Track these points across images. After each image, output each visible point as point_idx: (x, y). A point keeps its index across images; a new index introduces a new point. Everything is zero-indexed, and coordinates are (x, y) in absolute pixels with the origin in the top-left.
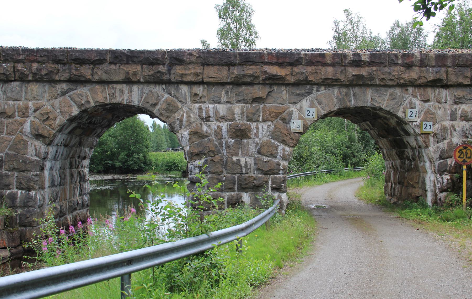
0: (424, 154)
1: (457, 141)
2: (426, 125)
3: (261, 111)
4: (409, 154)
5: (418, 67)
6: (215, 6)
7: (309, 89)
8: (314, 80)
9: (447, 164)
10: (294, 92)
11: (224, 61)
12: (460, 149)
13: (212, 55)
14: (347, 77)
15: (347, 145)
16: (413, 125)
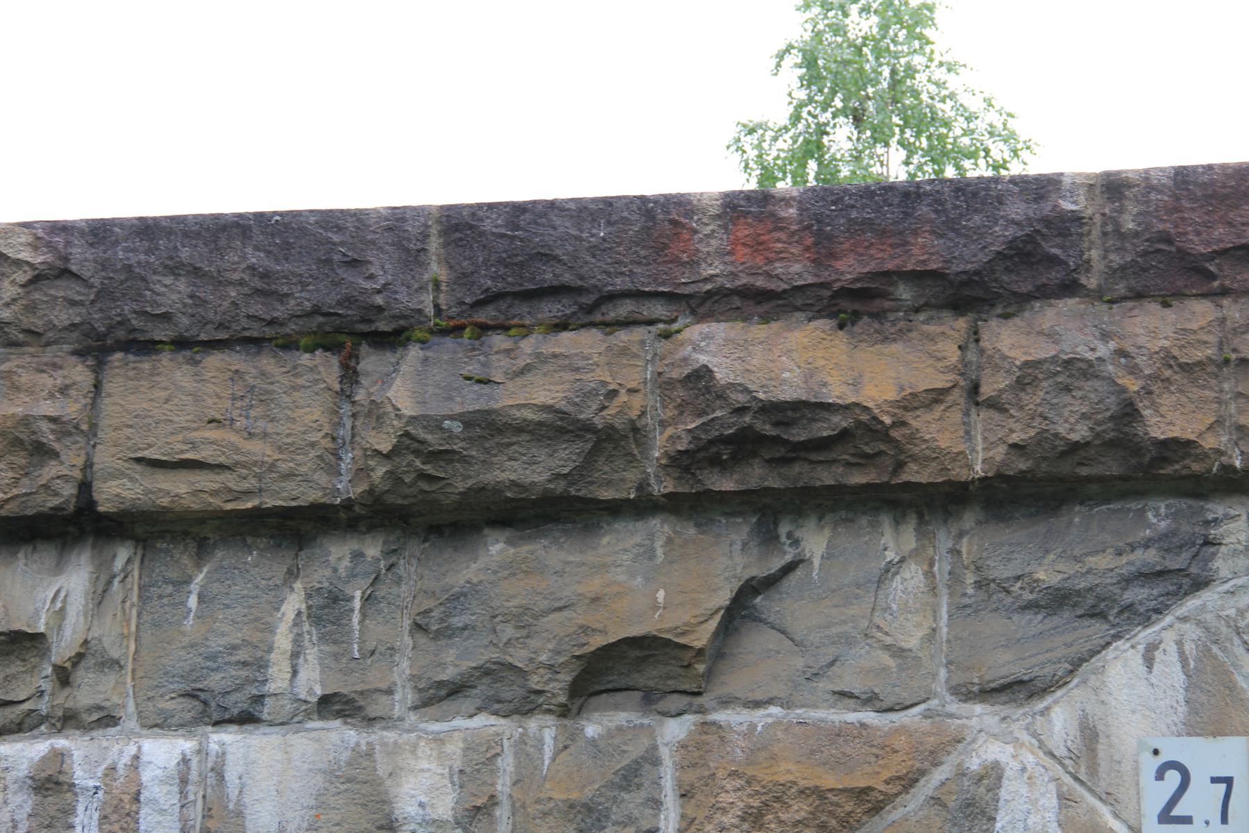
3: (668, 784)
6: (732, 132)
7: (1165, 541)
8: (1209, 442)
10: (1001, 571)
11: (302, 299)
13: (185, 254)
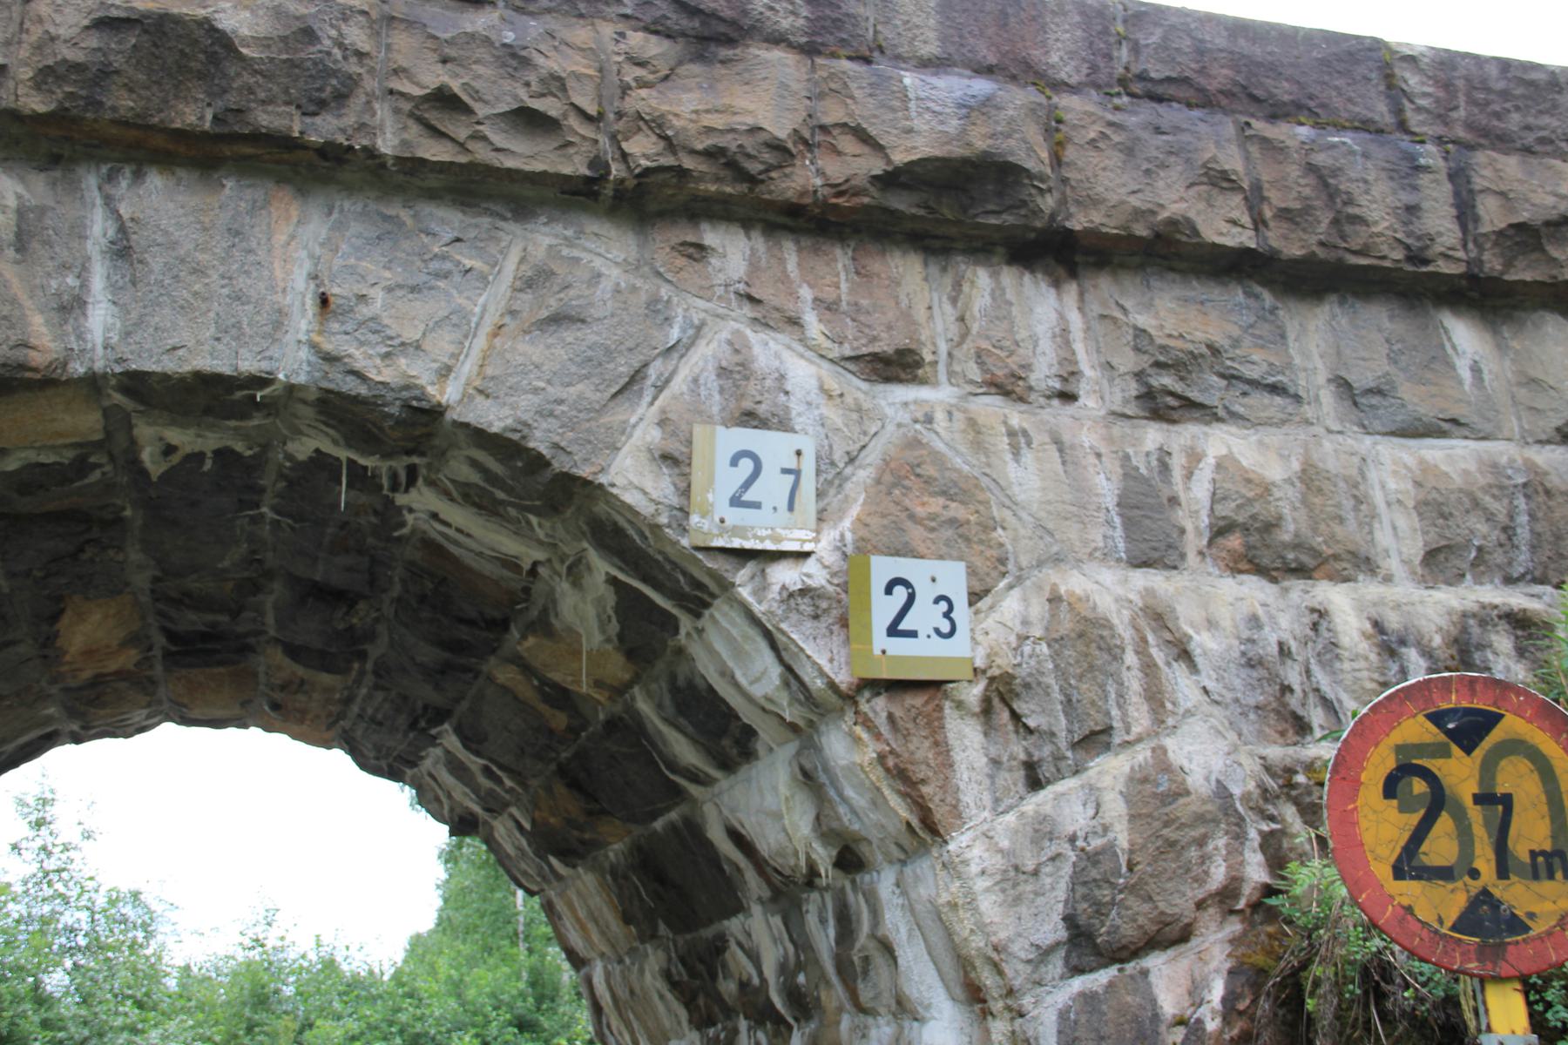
0: (896, 923)
1: (1218, 764)
2: (900, 593)
4: (755, 958)
5: (791, 46)
9: (1156, 1017)
12: (1400, 749)
14: (36, 32)
15: (520, 1011)
16: (774, 592)
